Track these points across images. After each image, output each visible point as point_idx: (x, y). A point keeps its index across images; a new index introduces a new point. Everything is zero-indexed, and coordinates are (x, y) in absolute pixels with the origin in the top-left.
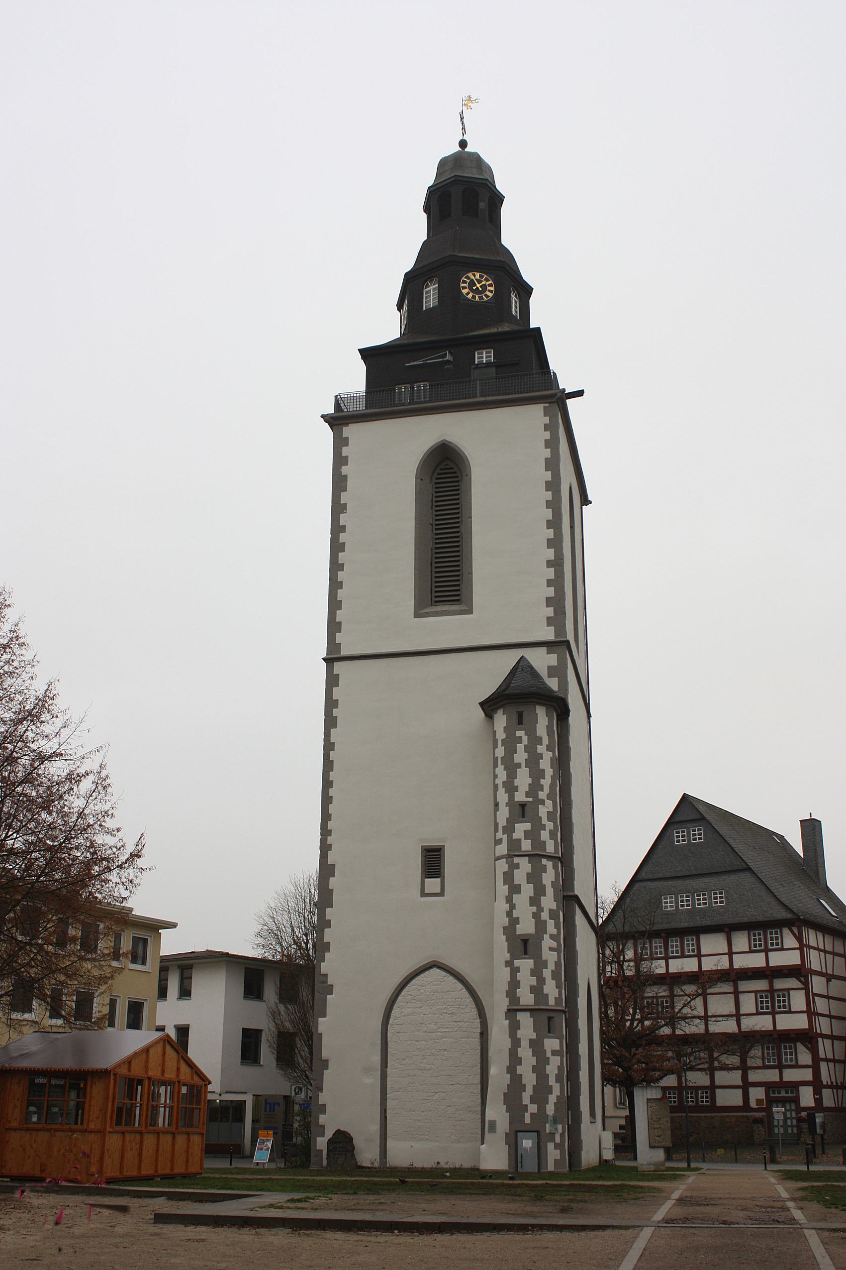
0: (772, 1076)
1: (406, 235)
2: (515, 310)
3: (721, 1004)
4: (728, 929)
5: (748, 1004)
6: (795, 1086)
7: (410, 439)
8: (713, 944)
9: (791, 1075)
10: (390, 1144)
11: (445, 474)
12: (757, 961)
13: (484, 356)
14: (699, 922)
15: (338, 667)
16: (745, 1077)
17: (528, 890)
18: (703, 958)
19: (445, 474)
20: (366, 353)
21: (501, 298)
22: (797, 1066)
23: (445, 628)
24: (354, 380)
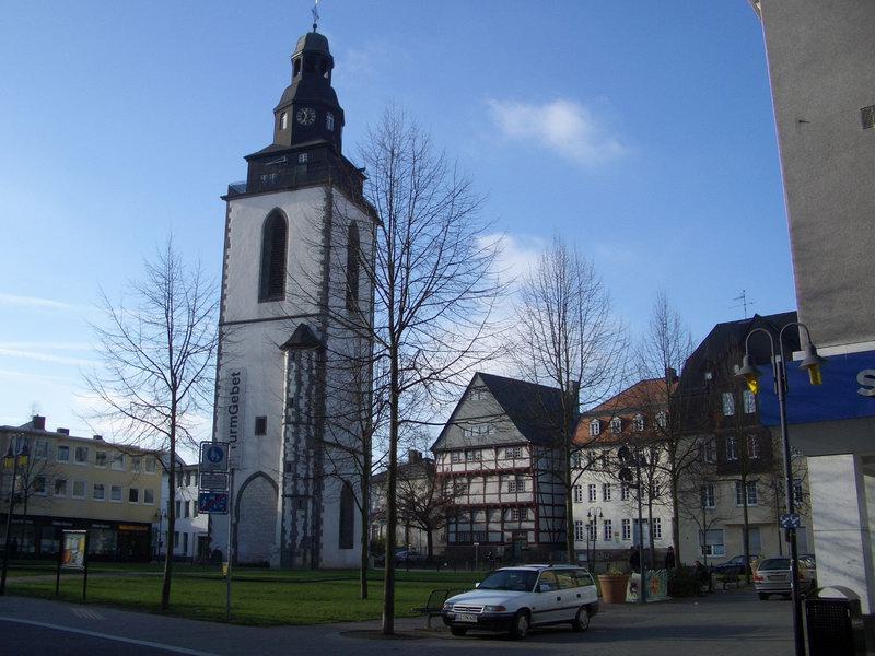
0: (516, 525)
1: (281, 80)
2: (330, 126)
3: (492, 486)
4: (497, 448)
5: (505, 488)
6: (526, 531)
7: (255, 212)
8: (488, 455)
9: (525, 525)
10: (854, 495)
11: (275, 229)
12: (509, 464)
13: (303, 157)
15: (225, 329)
16: (502, 527)
17: (292, 440)
19: (275, 229)
20: (248, 158)
21: (321, 120)
22: (528, 521)
23: (270, 309)
24: (240, 175)
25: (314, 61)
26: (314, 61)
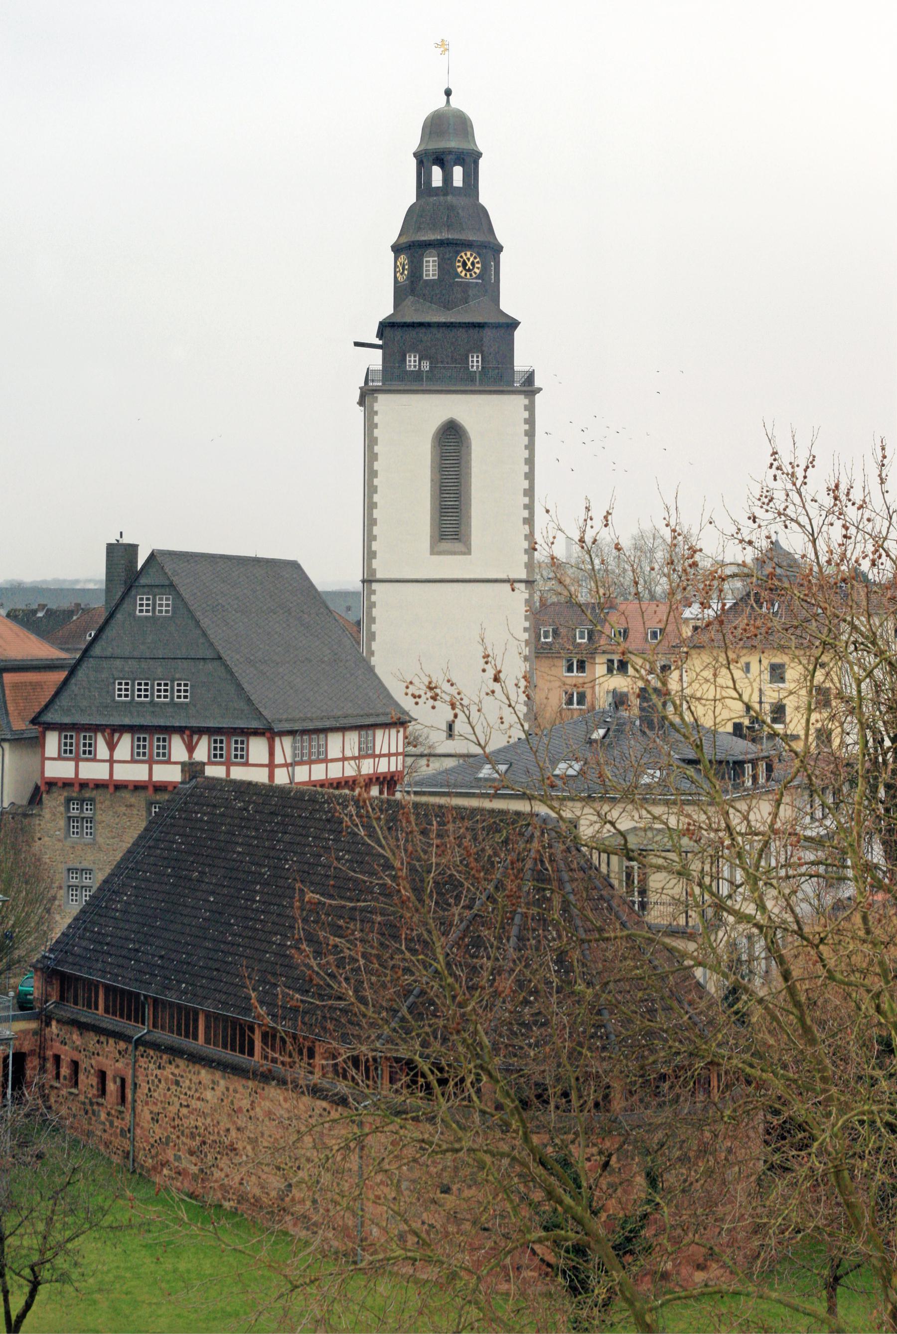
4: (191, 734)
7: (417, 417)
18: (115, 765)
25: (447, 148)
26: (447, 148)
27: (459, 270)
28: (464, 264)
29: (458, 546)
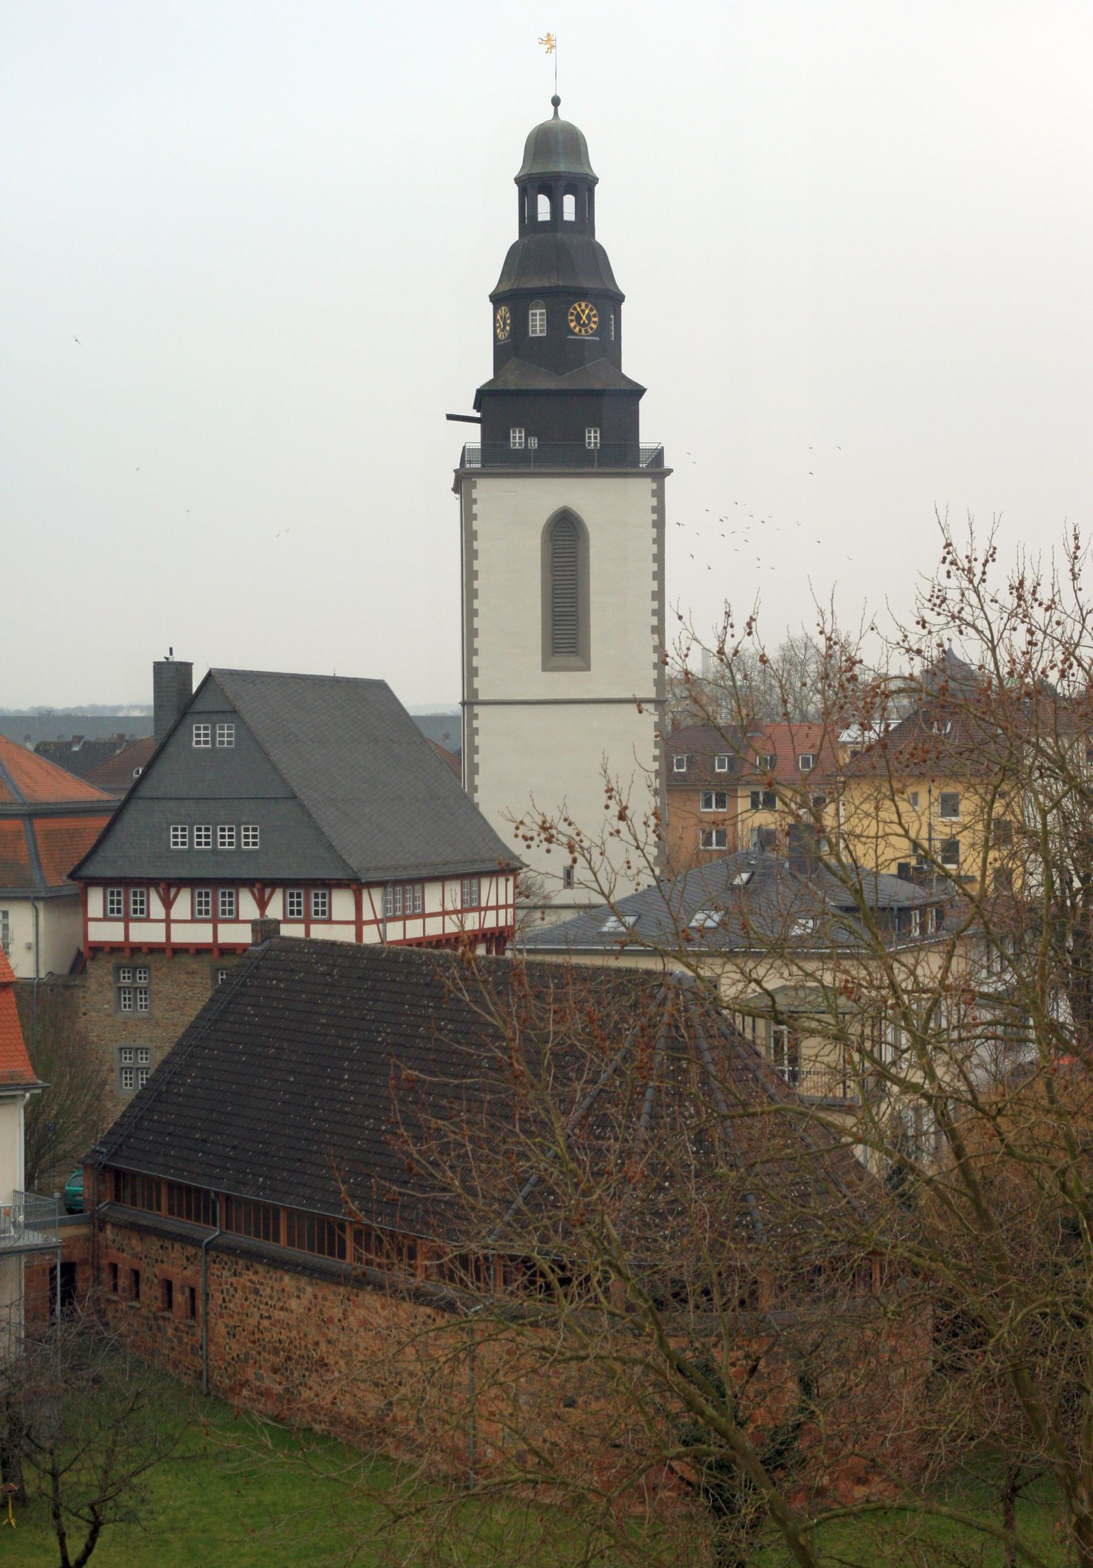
4: (261, 887)
7: (524, 505)
14: (424, 873)
25: (555, 168)
26: (555, 168)
27: (572, 325)
28: (578, 318)
29: (574, 660)
